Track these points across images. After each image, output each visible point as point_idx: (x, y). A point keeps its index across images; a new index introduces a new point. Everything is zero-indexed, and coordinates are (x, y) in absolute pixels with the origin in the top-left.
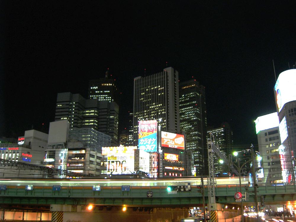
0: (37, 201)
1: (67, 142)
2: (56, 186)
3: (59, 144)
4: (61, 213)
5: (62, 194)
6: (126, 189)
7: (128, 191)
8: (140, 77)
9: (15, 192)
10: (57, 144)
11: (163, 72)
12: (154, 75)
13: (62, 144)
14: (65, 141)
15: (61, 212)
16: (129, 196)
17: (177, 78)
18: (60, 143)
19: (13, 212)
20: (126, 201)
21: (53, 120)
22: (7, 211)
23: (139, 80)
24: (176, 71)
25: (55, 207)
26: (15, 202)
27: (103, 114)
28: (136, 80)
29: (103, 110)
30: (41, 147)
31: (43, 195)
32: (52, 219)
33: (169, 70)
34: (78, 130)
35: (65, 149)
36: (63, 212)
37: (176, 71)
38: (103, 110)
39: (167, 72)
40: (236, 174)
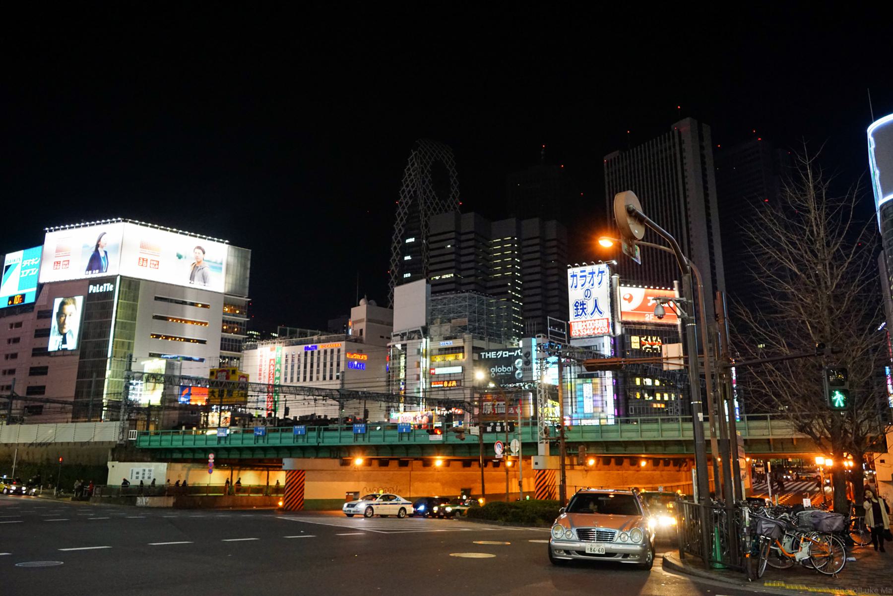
0: (251, 453)
1: (427, 324)
2: (403, 425)
3: (412, 330)
4: (300, 472)
5: (684, 432)
6: (299, 432)
7: (409, 433)
8: (616, 153)
9: (658, 431)
10: (410, 330)
11: (671, 133)
12: (637, 150)
13: (419, 330)
14: (424, 324)
15: (299, 471)
16: (366, 443)
17: (707, 143)
18: (415, 328)
19: (259, 472)
20: (592, 450)
21: (355, 306)
22: (248, 470)
23: (615, 158)
24: (704, 125)
25: (288, 462)
26: (247, 456)
27: (530, 249)
28: (607, 162)
29: (530, 242)
30: (385, 337)
31: (160, 445)
32: (304, 485)
33: (685, 127)
34: (446, 298)
35: (424, 340)
36: (303, 471)
37: (704, 125)
38: (530, 242)
39: (679, 133)
40: (49, 441)
